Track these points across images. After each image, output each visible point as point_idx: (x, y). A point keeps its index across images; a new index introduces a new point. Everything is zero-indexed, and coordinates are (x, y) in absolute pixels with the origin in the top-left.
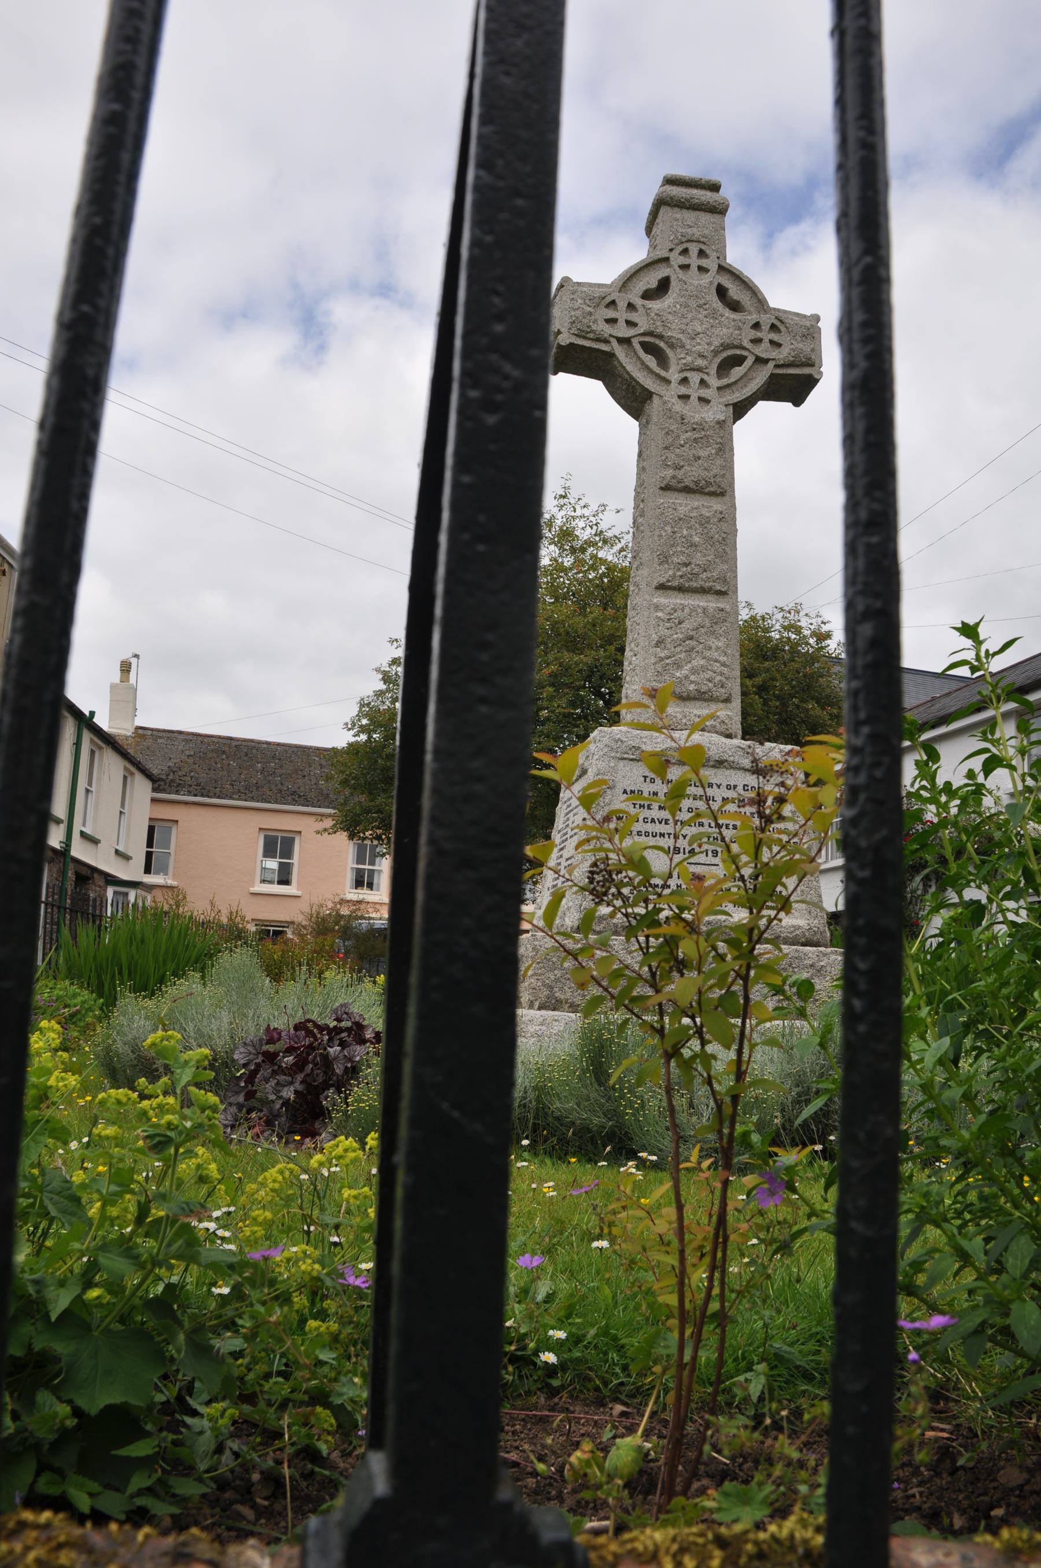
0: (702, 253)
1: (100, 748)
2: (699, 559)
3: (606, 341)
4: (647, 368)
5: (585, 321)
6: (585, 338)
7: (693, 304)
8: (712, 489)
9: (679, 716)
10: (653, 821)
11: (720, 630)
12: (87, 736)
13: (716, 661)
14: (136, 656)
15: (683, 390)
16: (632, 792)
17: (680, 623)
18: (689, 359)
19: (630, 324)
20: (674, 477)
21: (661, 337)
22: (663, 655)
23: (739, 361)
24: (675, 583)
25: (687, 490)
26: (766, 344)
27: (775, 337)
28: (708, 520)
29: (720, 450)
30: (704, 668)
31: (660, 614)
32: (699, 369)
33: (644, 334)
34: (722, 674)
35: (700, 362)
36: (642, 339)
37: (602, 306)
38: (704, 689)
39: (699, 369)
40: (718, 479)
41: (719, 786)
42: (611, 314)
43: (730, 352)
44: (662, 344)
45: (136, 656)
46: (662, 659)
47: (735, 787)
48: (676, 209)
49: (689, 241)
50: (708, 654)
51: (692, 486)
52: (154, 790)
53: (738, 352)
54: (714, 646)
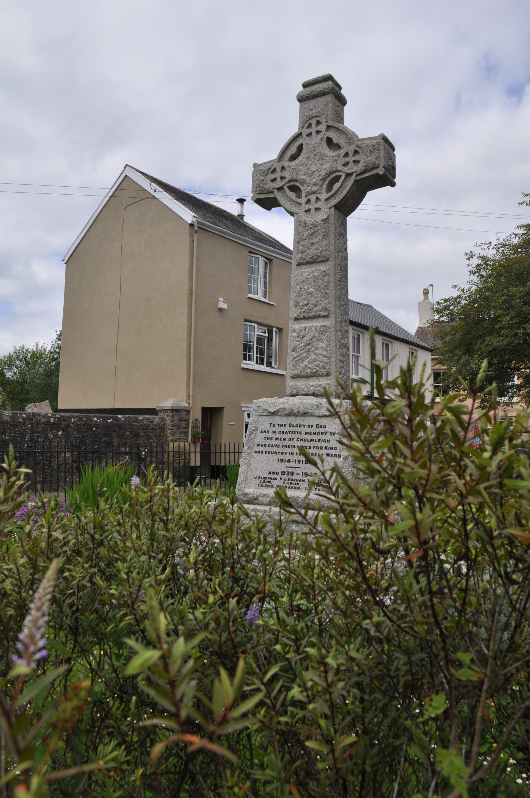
0: (318, 123)
1: (391, 342)
2: (313, 301)
3: (272, 192)
4: (291, 200)
5: (261, 185)
6: (263, 194)
7: (312, 155)
8: (320, 259)
9: (303, 387)
10: (272, 446)
11: (323, 337)
12: (379, 341)
13: (321, 355)
14: (432, 285)
15: (308, 207)
16: (265, 432)
17: (303, 337)
18: (309, 188)
19: (282, 178)
20: (301, 258)
21: (296, 180)
22: (295, 356)
23: (336, 179)
24: (302, 316)
25: (308, 263)
26: (351, 164)
27: (356, 158)
28: (317, 278)
29: (325, 235)
30: (314, 360)
31: (294, 334)
32: (314, 193)
33: (289, 182)
34: (323, 362)
35: (315, 188)
36: (288, 185)
37: (269, 174)
38: (314, 371)
39: (314, 193)
40: (323, 253)
41: (304, 426)
42: (273, 176)
43: (332, 176)
44: (298, 184)
45: (432, 285)
46: (295, 358)
47: (312, 426)
48: (307, 102)
49: (310, 119)
50: (317, 351)
51: (310, 260)
52: (432, 355)
53: (336, 174)
54: (320, 347)
